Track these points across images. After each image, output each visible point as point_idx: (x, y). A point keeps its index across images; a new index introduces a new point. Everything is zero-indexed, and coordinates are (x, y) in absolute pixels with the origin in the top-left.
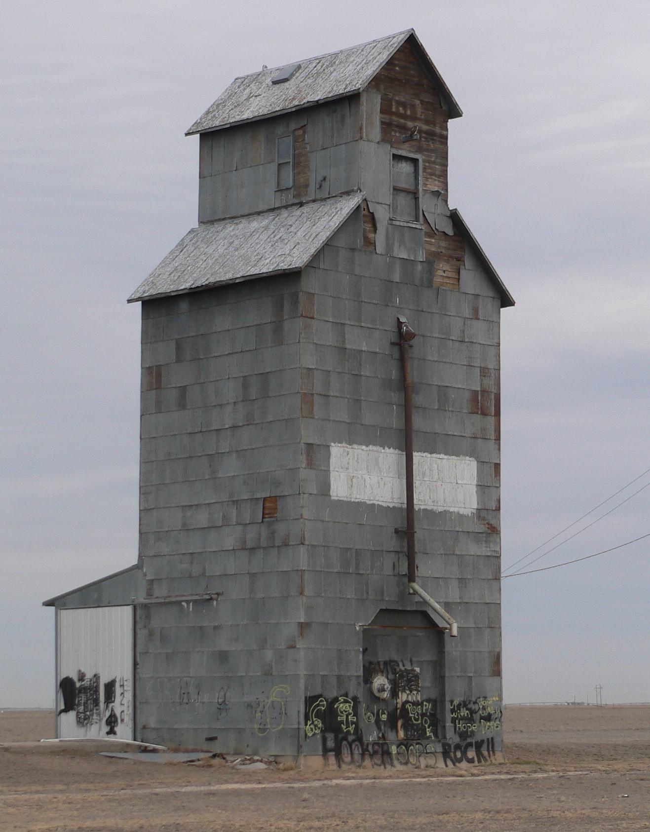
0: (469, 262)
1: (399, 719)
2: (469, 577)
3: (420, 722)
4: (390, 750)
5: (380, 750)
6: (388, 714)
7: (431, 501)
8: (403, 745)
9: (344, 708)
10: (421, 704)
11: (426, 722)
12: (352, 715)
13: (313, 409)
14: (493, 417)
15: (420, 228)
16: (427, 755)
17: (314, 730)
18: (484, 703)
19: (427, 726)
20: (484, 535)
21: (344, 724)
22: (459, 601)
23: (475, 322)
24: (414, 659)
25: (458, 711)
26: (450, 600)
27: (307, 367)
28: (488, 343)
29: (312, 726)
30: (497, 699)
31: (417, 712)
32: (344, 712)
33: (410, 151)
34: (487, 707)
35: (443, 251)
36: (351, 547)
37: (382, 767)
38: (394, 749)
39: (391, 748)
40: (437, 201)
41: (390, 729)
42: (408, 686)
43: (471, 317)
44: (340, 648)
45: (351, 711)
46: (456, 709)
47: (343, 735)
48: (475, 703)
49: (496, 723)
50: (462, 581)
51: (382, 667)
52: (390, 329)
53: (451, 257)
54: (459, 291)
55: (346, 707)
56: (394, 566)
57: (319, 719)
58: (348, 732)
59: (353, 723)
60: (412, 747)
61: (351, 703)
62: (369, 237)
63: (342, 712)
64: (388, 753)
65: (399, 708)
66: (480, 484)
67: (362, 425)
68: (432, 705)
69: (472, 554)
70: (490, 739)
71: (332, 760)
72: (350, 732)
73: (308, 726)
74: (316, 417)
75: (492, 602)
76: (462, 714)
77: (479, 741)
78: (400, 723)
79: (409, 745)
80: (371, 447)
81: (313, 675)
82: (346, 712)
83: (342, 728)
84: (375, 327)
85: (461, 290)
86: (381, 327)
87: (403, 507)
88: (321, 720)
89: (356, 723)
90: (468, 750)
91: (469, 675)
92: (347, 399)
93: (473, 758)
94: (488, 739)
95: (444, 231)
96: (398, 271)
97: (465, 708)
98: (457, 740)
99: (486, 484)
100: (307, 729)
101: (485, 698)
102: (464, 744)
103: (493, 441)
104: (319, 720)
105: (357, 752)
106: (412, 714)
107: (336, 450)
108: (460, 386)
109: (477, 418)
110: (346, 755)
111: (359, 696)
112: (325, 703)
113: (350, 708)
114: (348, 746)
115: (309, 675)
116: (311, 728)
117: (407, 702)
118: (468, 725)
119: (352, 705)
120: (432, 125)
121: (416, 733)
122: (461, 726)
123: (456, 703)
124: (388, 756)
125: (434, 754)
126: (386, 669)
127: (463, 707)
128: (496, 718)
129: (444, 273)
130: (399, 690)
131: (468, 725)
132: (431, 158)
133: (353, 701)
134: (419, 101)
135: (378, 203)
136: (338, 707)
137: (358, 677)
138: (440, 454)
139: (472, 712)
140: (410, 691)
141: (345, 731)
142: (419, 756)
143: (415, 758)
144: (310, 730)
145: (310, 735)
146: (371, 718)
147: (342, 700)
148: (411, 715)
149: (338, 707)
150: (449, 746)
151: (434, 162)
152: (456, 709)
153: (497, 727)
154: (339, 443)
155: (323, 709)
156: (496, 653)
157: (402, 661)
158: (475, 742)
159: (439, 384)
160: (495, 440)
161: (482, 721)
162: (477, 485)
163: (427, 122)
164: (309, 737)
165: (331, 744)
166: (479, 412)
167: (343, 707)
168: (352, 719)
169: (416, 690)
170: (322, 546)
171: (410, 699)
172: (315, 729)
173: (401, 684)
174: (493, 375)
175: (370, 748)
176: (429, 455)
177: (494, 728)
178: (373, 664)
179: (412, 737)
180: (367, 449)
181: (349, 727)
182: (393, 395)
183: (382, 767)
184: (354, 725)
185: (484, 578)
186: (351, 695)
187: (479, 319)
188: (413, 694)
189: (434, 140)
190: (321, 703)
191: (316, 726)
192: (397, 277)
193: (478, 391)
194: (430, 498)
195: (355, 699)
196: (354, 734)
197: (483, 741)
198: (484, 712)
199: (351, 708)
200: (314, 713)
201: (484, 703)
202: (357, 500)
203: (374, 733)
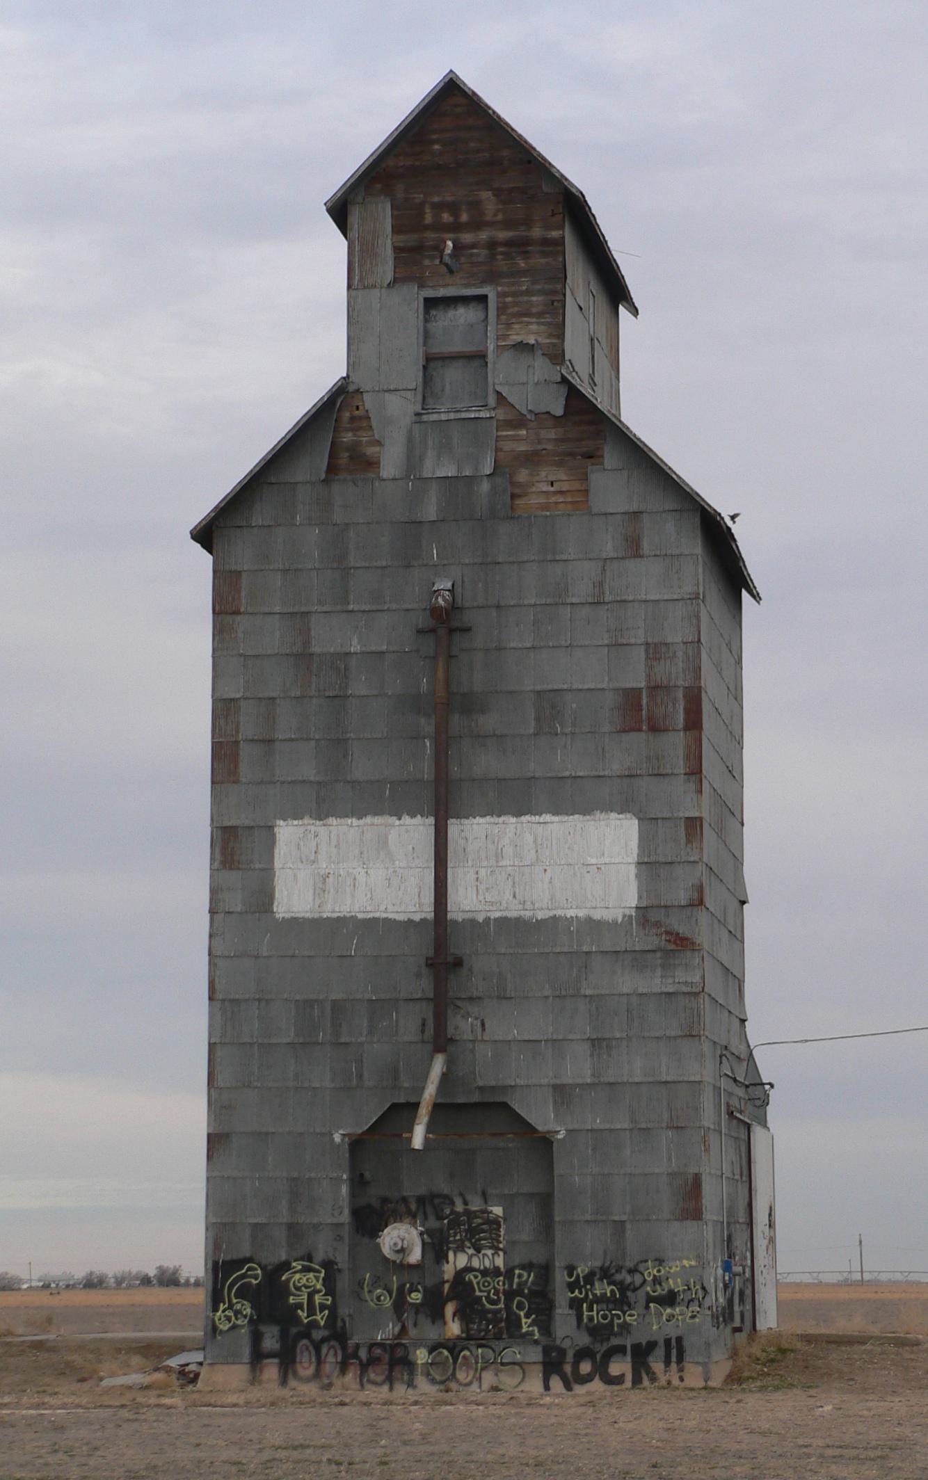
0: (611, 457)
1: (449, 1299)
2: (618, 1035)
3: (502, 1305)
4: (411, 1357)
5: (386, 1357)
6: (424, 1291)
7: (517, 902)
8: (444, 1348)
9: (304, 1281)
10: (509, 1273)
11: (520, 1306)
12: (321, 1294)
13: (236, 767)
14: (682, 733)
15: (488, 416)
16: (502, 1368)
17: (233, 1318)
18: (659, 1271)
19: (522, 1314)
20: (659, 954)
21: (303, 1311)
22: (589, 1081)
23: (632, 565)
24: (490, 1191)
25: (588, 1287)
26: (568, 1079)
27: (224, 697)
28: (666, 597)
29: (230, 1313)
30: (693, 1263)
31: (494, 1288)
32: (303, 1289)
33: (467, 286)
34: (667, 1279)
35: (549, 447)
36: (321, 997)
37: (386, 1387)
38: (421, 1356)
39: (415, 1352)
40: (534, 359)
41: (429, 1321)
42: (470, 1240)
43: (620, 556)
44: (295, 1175)
45: (319, 1286)
46: (582, 1283)
47: (302, 1329)
48: (632, 1271)
49: (690, 1309)
50: (597, 1043)
51: (413, 1207)
52: (415, 606)
53: (572, 455)
54: (591, 514)
55: (307, 1280)
56: (424, 1025)
57: (245, 1300)
58: (313, 1325)
59: (323, 1307)
60: (466, 1353)
61: (319, 1272)
62: (368, 453)
63: (298, 1289)
64: (407, 1364)
65: (448, 1281)
66: (646, 860)
67: (474, 780)
68: (535, 1276)
69: (625, 990)
70: (674, 1343)
71: (271, 1371)
72: (319, 1324)
73: (219, 1314)
74: (244, 780)
75: (681, 1079)
76: (598, 1292)
77: (644, 1344)
78: (450, 1309)
79: (457, 1349)
80: (369, 819)
81: (233, 1224)
82: (307, 1287)
83: (300, 1317)
84: (380, 608)
85: (595, 510)
86: (394, 606)
87: (428, 917)
88: (251, 1302)
89: (333, 1310)
90: (612, 1360)
91: (616, 1218)
92: (314, 742)
93: (623, 1375)
94: (668, 1342)
95: (548, 410)
96: (434, 500)
97: (605, 1281)
98: (584, 1340)
99: (662, 859)
100: (216, 1319)
101: (660, 1261)
102: (601, 1349)
103: (682, 776)
104: (245, 1302)
105: (331, 1359)
106: (481, 1291)
107: (287, 833)
108: (592, 686)
109: (638, 740)
110: (306, 1365)
111: (339, 1259)
112: (259, 1272)
113: (318, 1281)
114: (311, 1348)
115: (225, 1224)
116: (225, 1316)
117: (468, 1269)
118: (614, 1312)
119: (322, 1275)
120: (523, 228)
121: (491, 1327)
122: (595, 1315)
123: (582, 1270)
124: (406, 1368)
125: (521, 1367)
126: (421, 1211)
127: (601, 1279)
128: (692, 1300)
129: (552, 485)
130: (449, 1249)
131: (614, 1312)
132: (521, 286)
133: (323, 1268)
134: (490, 193)
135: (389, 391)
136: (288, 1280)
137: (338, 1225)
138: (540, 815)
139: (623, 1288)
140: (475, 1250)
141: (306, 1321)
142: (483, 1369)
143: (471, 1373)
144: (223, 1319)
145: (226, 1328)
146: (382, 1298)
147: (300, 1267)
148: (478, 1293)
149: (288, 1280)
150: (562, 1352)
151: (528, 292)
152: (582, 1283)
153: (693, 1317)
154: (295, 820)
155: (254, 1282)
156: (690, 1178)
157: (461, 1195)
158: (633, 1346)
159: (539, 688)
160: (685, 774)
161: (652, 1305)
162: (638, 863)
163: (508, 224)
164: (221, 1331)
165: (270, 1341)
166: (644, 727)
167: (301, 1279)
168: (320, 1301)
169: (490, 1248)
170: (255, 1000)
171: (475, 1263)
172: (237, 1319)
173: (455, 1236)
174: (680, 654)
175: (363, 1353)
176: (513, 820)
177: (684, 1320)
178: (391, 1203)
179: (483, 1334)
180: (361, 822)
181: (315, 1315)
182: (423, 721)
183: (386, 1387)
184: (326, 1312)
185: (657, 1034)
186: (320, 1256)
187: (641, 557)
188: (484, 1255)
189: (527, 252)
190: (249, 1273)
191: (237, 1313)
192: (431, 511)
193: (640, 689)
194: (514, 897)
195: (328, 1265)
196: (325, 1327)
197: (652, 1345)
198: (658, 1287)
199: (321, 1281)
200: (234, 1291)
201: (659, 1271)
202: (335, 915)
203: (388, 1326)
